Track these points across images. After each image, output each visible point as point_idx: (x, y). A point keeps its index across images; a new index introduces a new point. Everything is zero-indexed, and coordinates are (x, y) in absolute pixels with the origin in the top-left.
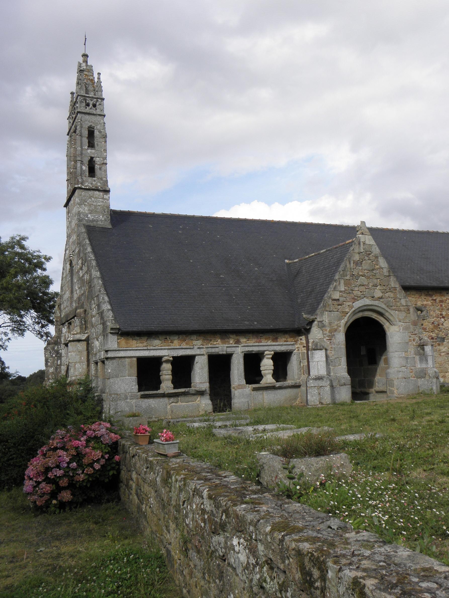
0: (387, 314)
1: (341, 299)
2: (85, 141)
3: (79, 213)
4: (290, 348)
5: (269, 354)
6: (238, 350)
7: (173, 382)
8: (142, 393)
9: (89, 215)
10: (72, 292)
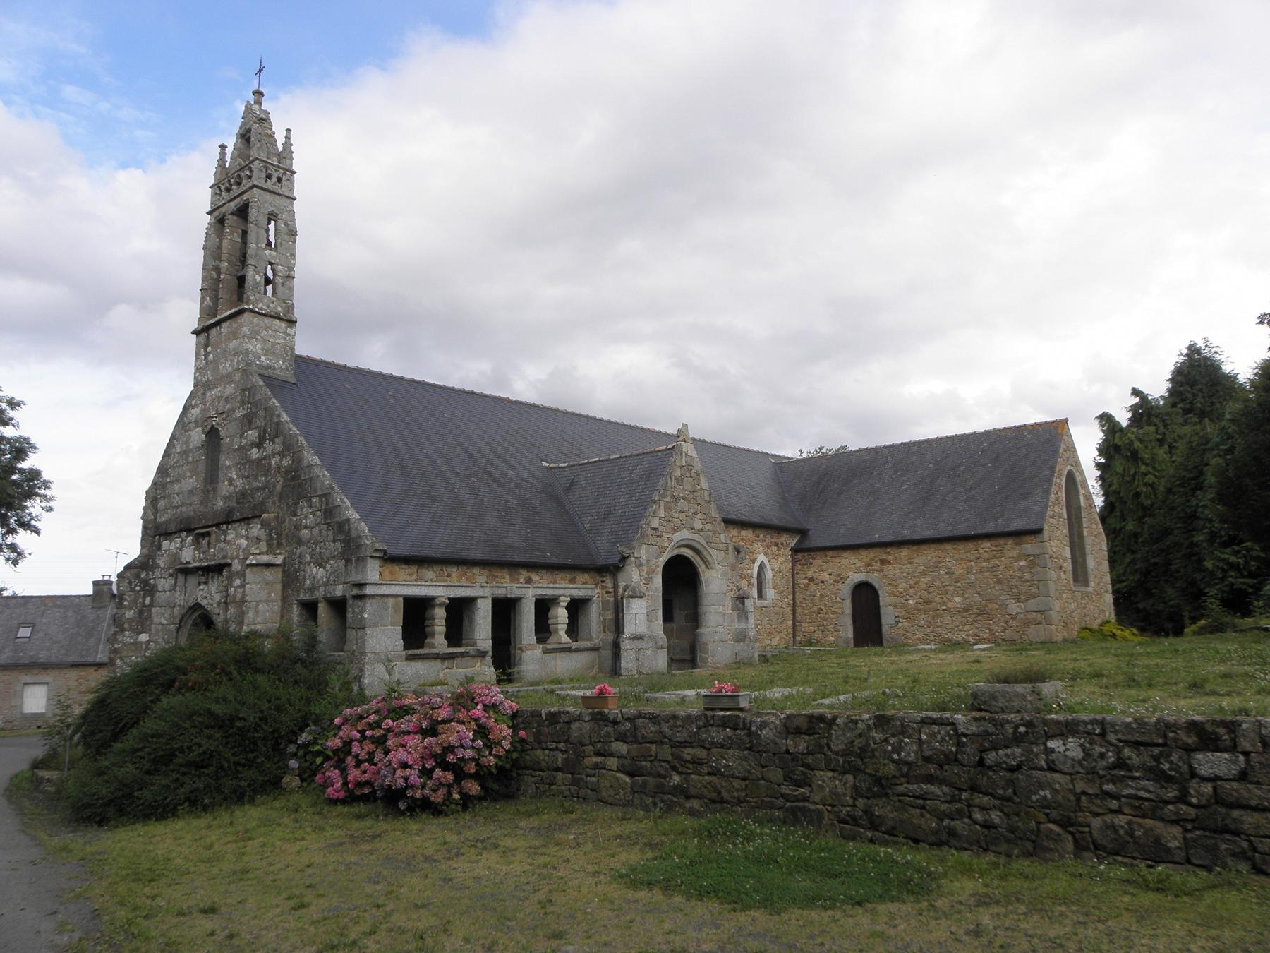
0: (705, 553)
1: (661, 528)
3: (247, 352)
4: (589, 593)
5: (564, 601)
6: (528, 590)
8: (410, 652)
10: (212, 477)
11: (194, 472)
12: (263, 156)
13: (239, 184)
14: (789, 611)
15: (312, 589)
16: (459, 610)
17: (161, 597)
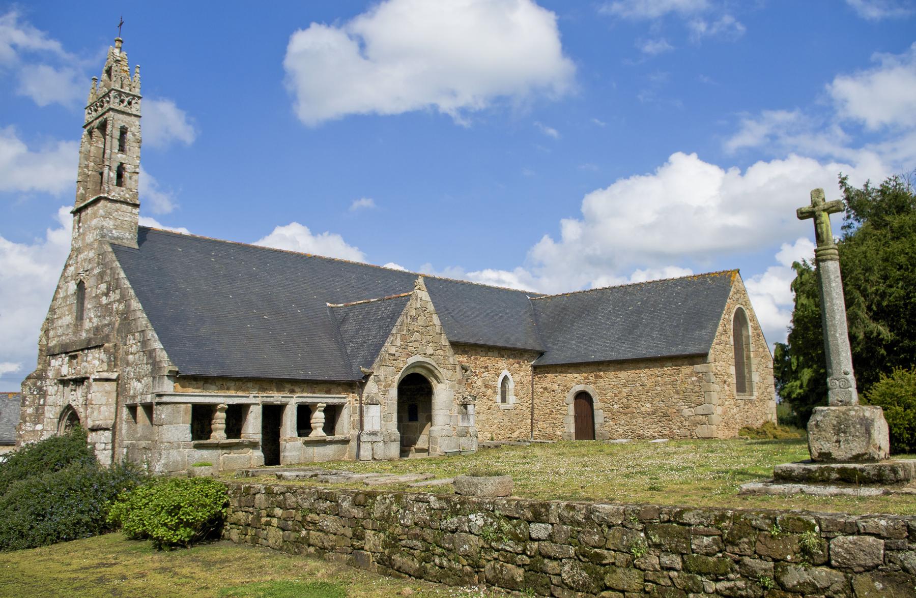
0: (436, 371)
1: (397, 354)
2: (116, 143)
3: (102, 228)
4: (342, 401)
6: (292, 402)
7: (226, 432)
8: (196, 442)
9: (114, 232)
10: (80, 317)
11: (71, 313)
12: (118, 87)
13: (102, 106)
14: (527, 412)
15: (134, 397)
16: (236, 414)
17: (50, 399)
